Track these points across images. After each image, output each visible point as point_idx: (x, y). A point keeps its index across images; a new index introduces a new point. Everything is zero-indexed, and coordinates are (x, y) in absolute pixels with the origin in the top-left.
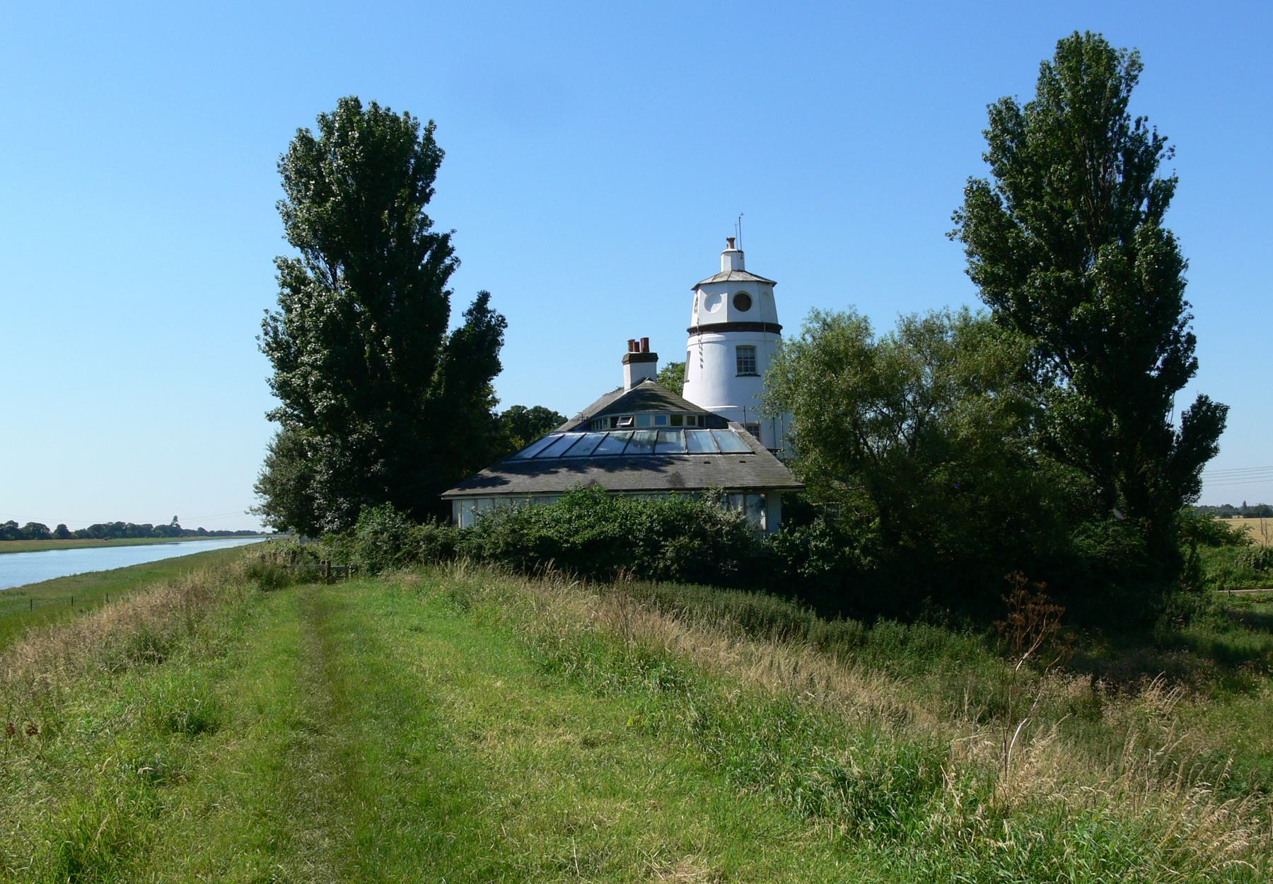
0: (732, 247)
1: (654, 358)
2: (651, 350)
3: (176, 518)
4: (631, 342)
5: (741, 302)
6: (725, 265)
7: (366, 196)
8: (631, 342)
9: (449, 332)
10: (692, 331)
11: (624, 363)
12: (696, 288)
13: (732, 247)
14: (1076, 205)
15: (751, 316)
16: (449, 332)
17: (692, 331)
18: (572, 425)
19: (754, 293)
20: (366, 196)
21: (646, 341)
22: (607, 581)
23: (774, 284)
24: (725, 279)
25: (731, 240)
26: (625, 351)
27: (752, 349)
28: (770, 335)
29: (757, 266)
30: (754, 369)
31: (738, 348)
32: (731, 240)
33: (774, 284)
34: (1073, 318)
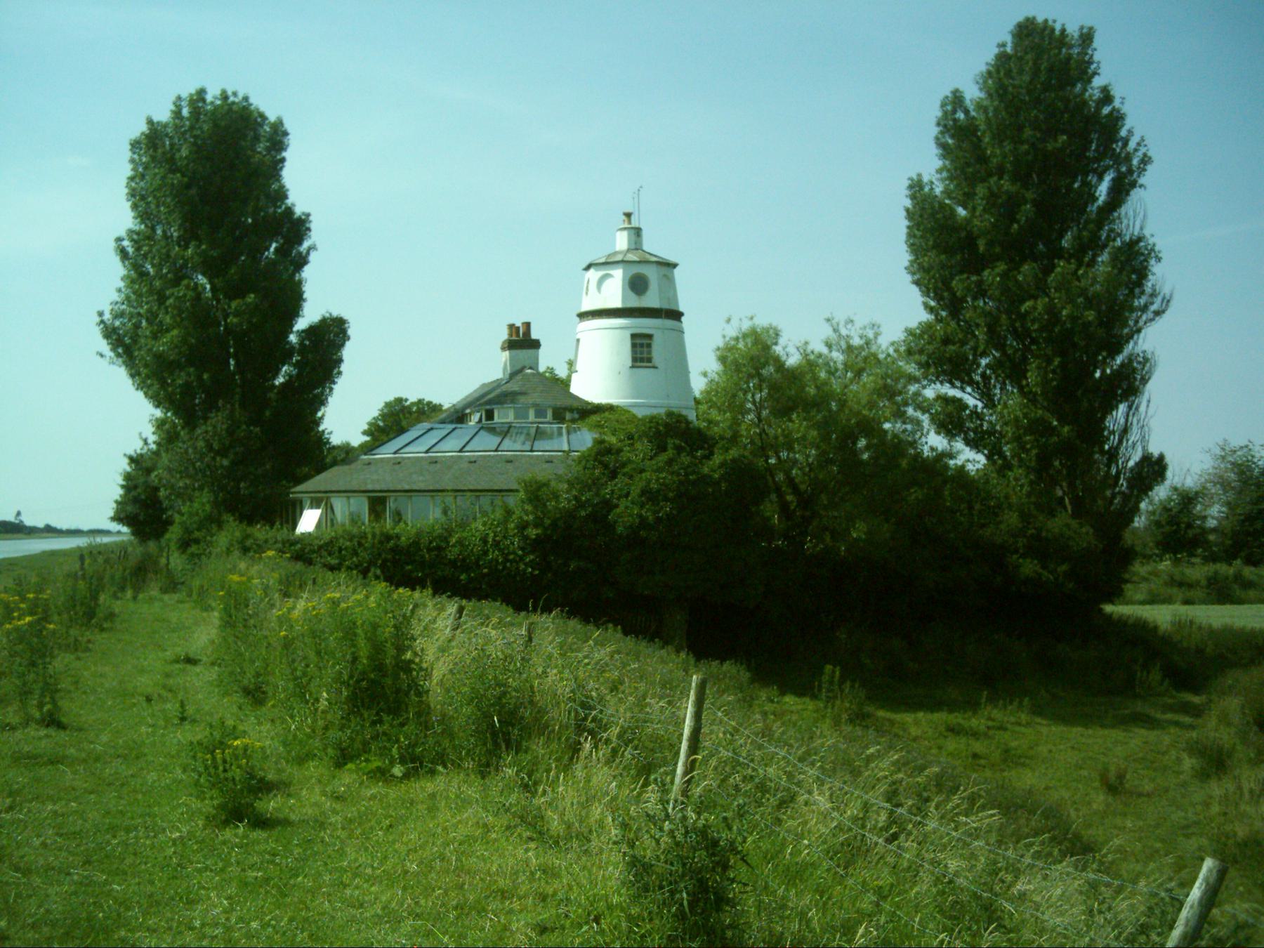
0: (630, 222)
1: (536, 345)
2: (534, 336)
3: (19, 514)
4: (511, 326)
5: (637, 284)
6: (622, 242)
7: (217, 209)
8: (511, 326)
9: (301, 324)
10: (583, 316)
11: (503, 349)
12: (588, 268)
13: (630, 222)
14: (1032, 198)
15: (651, 300)
16: (301, 324)
17: (583, 316)
18: (443, 416)
19: (652, 273)
20: (217, 209)
21: (528, 325)
22: (353, 699)
23: (675, 266)
24: (619, 258)
25: (628, 215)
26: (504, 335)
27: (650, 337)
28: (669, 323)
29: (654, 245)
30: (649, 360)
31: (633, 336)
32: (628, 215)
33: (675, 266)
34: (865, 456)
